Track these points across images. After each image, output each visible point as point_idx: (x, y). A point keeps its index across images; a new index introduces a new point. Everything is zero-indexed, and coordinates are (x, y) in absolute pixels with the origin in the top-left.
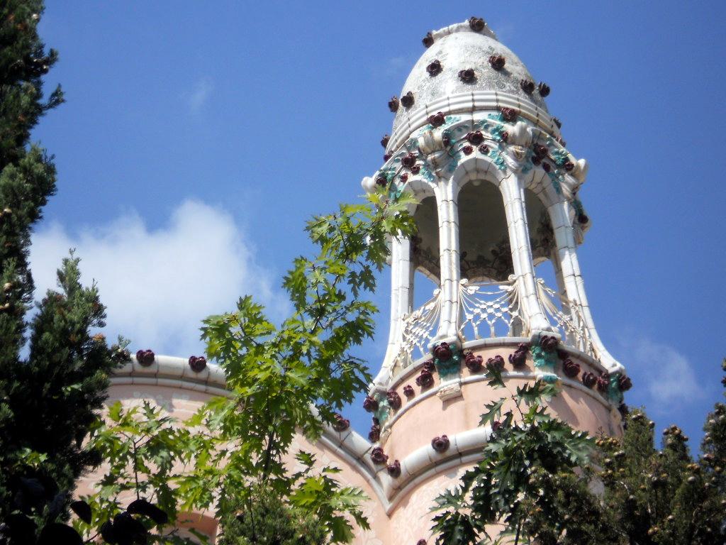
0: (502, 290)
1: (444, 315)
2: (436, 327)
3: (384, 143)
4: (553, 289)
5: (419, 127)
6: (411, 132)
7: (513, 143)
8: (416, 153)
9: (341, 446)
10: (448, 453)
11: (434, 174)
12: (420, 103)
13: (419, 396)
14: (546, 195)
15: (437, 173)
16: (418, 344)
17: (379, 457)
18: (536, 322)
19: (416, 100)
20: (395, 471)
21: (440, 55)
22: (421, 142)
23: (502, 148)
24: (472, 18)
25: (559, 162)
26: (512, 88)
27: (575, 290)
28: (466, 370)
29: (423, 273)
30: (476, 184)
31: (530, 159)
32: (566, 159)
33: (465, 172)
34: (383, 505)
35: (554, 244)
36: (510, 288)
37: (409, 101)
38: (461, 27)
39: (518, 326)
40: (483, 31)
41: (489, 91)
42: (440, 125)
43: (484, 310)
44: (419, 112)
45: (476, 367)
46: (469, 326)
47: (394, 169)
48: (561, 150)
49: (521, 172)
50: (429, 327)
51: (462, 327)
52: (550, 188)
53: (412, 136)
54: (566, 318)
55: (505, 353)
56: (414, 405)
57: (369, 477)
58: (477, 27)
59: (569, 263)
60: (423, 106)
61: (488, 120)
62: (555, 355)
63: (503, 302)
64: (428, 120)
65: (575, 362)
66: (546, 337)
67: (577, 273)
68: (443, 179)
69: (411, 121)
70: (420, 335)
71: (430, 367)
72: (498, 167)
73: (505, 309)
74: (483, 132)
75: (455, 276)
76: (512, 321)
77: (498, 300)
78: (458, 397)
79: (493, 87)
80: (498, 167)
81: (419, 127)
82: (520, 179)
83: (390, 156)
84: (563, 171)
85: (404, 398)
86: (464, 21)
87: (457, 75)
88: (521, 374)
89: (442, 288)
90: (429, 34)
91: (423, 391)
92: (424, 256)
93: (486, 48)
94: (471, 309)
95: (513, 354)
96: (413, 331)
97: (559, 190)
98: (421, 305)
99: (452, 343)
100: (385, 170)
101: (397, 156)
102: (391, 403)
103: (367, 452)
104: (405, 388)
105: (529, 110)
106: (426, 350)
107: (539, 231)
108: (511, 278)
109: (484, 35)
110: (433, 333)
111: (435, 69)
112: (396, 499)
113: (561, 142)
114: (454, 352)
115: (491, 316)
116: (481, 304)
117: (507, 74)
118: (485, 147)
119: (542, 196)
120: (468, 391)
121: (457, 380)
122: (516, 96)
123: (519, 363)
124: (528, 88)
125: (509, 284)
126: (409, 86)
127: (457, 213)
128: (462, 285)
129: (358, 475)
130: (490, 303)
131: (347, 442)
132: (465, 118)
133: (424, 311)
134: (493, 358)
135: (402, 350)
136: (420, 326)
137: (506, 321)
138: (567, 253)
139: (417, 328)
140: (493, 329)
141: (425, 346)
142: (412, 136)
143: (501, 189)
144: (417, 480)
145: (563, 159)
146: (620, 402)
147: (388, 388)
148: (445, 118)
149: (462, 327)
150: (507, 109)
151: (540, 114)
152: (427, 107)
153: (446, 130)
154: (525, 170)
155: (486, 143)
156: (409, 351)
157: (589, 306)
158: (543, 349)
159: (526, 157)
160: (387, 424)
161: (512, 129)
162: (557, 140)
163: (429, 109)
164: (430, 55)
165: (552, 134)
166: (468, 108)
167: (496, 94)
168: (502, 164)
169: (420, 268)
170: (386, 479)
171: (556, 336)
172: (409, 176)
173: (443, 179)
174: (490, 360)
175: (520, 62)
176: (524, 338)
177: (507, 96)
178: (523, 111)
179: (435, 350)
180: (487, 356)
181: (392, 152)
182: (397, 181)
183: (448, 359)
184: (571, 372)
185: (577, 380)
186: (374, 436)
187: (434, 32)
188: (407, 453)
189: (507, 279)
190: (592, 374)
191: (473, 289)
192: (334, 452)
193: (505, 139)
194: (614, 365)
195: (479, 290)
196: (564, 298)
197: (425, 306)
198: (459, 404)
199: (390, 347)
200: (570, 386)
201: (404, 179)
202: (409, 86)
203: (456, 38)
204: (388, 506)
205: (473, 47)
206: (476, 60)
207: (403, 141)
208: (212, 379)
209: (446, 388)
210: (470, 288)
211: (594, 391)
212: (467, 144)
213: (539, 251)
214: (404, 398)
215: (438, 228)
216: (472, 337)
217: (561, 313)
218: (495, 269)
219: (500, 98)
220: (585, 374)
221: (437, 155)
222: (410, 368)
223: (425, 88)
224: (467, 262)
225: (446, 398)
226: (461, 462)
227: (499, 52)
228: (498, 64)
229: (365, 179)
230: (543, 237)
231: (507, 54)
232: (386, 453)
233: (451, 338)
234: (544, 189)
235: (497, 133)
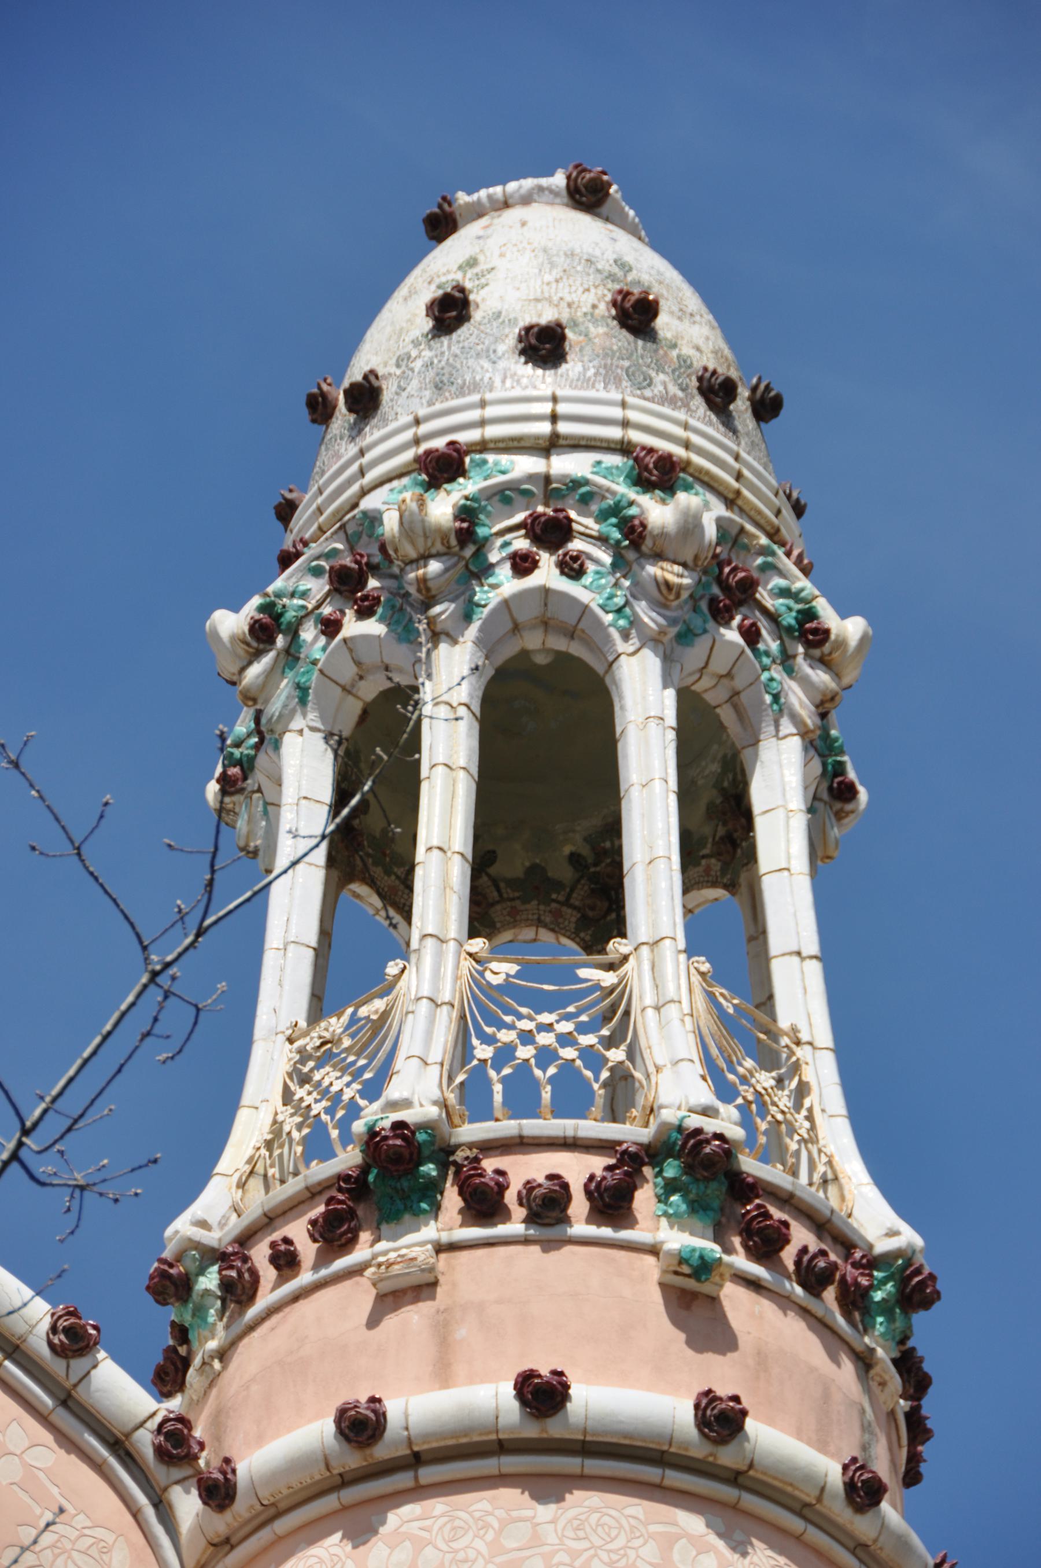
0: (587, 980)
1: (410, 1043)
2: (385, 1073)
3: (286, 511)
4: (734, 990)
6: (364, 492)
10: (382, 1452)
12: (399, 407)
14: (738, 709)
16: (325, 1117)
17: (176, 1443)
18: (679, 1089)
19: (386, 396)
20: (218, 1492)
21: (470, 273)
24: (576, 167)
26: (673, 390)
27: (801, 997)
29: (364, 898)
30: (541, 660)
31: (704, 605)
32: (809, 614)
33: (510, 626)
35: (751, 856)
36: (608, 979)
37: (365, 399)
38: (541, 189)
39: (622, 1093)
40: (604, 210)
41: (602, 394)
42: (452, 480)
43: (526, 1038)
47: (304, 595)
48: (798, 585)
49: (673, 645)
50: (363, 1069)
53: (368, 503)
54: (765, 1080)
56: (296, 1297)
58: (587, 196)
60: (406, 419)
63: (584, 1018)
64: (417, 459)
66: (698, 1131)
67: (812, 946)
68: (443, 637)
69: (369, 456)
70: (334, 1089)
71: (353, 1186)
73: (588, 1040)
74: (573, 514)
76: (605, 1074)
77: (571, 1009)
78: (422, 1288)
79: (618, 382)
80: (608, 618)
82: (667, 660)
83: (298, 555)
86: (552, 175)
89: (413, 958)
91: (323, 1259)
92: (369, 851)
93: (605, 263)
94: (489, 1030)
96: (317, 1076)
98: (347, 1005)
99: (426, 1126)
100: (279, 595)
101: (318, 558)
102: (227, 1285)
103: (142, 1425)
104: (273, 1245)
106: (346, 1138)
107: (712, 812)
108: (617, 946)
109: (607, 220)
110: (372, 1090)
111: (450, 311)
113: (799, 562)
114: (426, 1152)
115: (545, 1056)
116: (520, 1017)
118: (575, 559)
119: (727, 715)
120: (462, 1274)
122: (681, 415)
124: (717, 393)
125: (611, 967)
126: (371, 356)
127: (174, 1516)
128: (470, 955)
130: (546, 1018)
133: (354, 1020)
134: (541, 1179)
135: (277, 1127)
136: (334, 1067)
137: (588, 1074)
139: (328, 1069)
140: (546, 1094)
141: (344, 1126)
142: (368, 503)
144: (281, 1526)
145: (799, 612)
146: (902, 1341)
149: (461, 1078)
150: (651, 451)
151: (746, 472)
152: (417, 422)
153: (467, 498)
154: (686, 636)
155: (577, 545)
156: (296, 1135)
159: (691, 596)
161: (658, 513)
162: (788, 554)
164: (441, 266)
165: (774, 534)
166: (537, 437)
167: (624, 405)
169: (357, 887)
170: (188, 1505)
171: (728, 1134)
172: (346, 620)
173: (443, 637)
174: (530, 1186)
175: (704, 310)
176: (632, 1133)
178: (697, 459)
179: (373, 1139)
180: (525, 1170)
181: (306, 544)
182: (309, 633)
183: (394, 1174)
184: (766, 1244)
186: (168, 1377)
187: (462, 198)
188: (260, 1440)
189: (603, 951)
190: (823, 1253)
191: (500, 971)
193: (634, 540)
195: (518, 975)
196: (761, 1016)
197: (358, 1007)
199: (243, 1116)
201: (331, 627)
202: (371, 356)
203: (524, 224)
205: (571, 255)
206: (574, 297)
207: (339, 515)
209: (392, 1255)
210: (494, 966)
212: (521, 543)
213: (708, 870)
214: (268, 1273)
217: (749, 1063)
218: (574, 908)
219: (633, 416)
220: (804, 1250)
222: (294, 1186)
223: (418, 365)
224: (495, 882)
225: (387, 1286)
227: (645, 278)
228: (637, 315)
230: (721, 831)
231: (668, 287)
233: (423, 1110)
235: (614, 520)
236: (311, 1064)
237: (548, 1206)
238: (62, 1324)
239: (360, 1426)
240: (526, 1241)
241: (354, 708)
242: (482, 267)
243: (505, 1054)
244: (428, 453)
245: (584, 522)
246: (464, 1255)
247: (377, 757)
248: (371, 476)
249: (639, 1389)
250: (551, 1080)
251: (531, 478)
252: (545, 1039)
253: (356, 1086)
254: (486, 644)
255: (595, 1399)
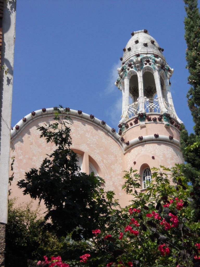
5: (133, 56)
6: (130, 58)
7: (158, 63)
8: (132, 63)
9: (113, 136)
10: (142, 141)
11: (137, 69)
13: (134, 125)
14: (164, 77)
15: (138, 69)
16: (134, 112)
17: (123, 140)
18: (164, 110)
19: (131, 49)
20: (128, 144)
22: (135, 60)
23: (154, 64)
25: (167, 69)
27: (170, 102)
28: (147, 120)
32: (169, 68)
34: (123, 152)
36: (157, 100)
37: (129, 49)
40: (147, 33)
43: (151, 106)
44: (132, 53)
45: (149, 120)
46: (147, 109)
47: (126, 67)
49: (159, 71)
50: (136, 108)
51: (146, 109)
52: (165, 75)
55: (157, 117)
56: (132, 128)
57: (120, 144)
58: (146, 32)
59: (169, 95)
61: (151, 57)
62: (169, 118)
65: (173, 120)
66: (167, 114)
67: (171, 98)
69: (131, 54)
71: (137, 119)
72: (153, 69)
73: (156, 106)
74: (150, 60)
75: (143, 96)
78: (145, 127)
79: (152, 48)
80: (153, 69)
81: (133, 56)
82: (159, 73)
84: (168, 71)
85: (129, 125)
87: (143, 44)
88: (161, 122)
90: (133, 32)
95: (159, 117)
97: (167, 76)
99: (144, 113)
104: (130, 123)
105: (160, 55)
111: (137, 42)
112: (127, 151)
115: (153, 107)
117: (155, 45)
120: (147, 125)
121: (144, 122)
122: (157, 51)
123: (160, 120)
124: (160, 49)
129: (117, 144)
130: (152, 104)
131: (115, 135)
132: (145, 55)
133: (135, 104)
138: (169, 92)
140: (153, 110)
143: (154, 75)
147: (125, 122)
148: (140, 55)
149: (146, 109)
152: (135, 51)
155: (150, 62)
157: (174, 106)
158: (166, 117)
160: (124, 131)
161: (158, 60)
163: (136, 52)
168: (154, 68)
174: (153, 118)
177: (143, 50)
179: (139, 115)
180: (152, 117)
182: (126, 70)
183: (142, 117)
184: (172, 123)
185: (152, 121)
186: (120, 134)
187: (135, 32)
192: (111, 137)
193: (156, 62)
194: (181, 122)
198: (145, 128)
200: (172, 126)
201: (129, 69)
204: (124, 152)
205: (146, 37)
208: (83, 116)
211: (177, 128)
212: (145, 62)
214: (129, 125)
215: (138, 83)
216: (148, 112)
219: (154, 51)
220: (175, 124)
221: (139, 64)
223: (134, 47)
226: (107, 133)
228: (153, 42)
229: (118, 68)
232: (124, 139)
233: (143, 112)
234: (163, 75)
236: (131, 107)
237: (155, 120)
238: (113, 129)
239: (141, 138)
240: (153, 123)
241: (131, 76)
242: (139, 38)
243: (150, 107)
244: (137, 54)
245: (151, 60)
246: (148, 124)
247: (134, 80)
248: (131, 56)
249: (164, 135)
250: (154, 109)
251: (146, 57)
252: (153, 106)
253: (136, 110)
254: (143, 72)
255: (161, 136)
